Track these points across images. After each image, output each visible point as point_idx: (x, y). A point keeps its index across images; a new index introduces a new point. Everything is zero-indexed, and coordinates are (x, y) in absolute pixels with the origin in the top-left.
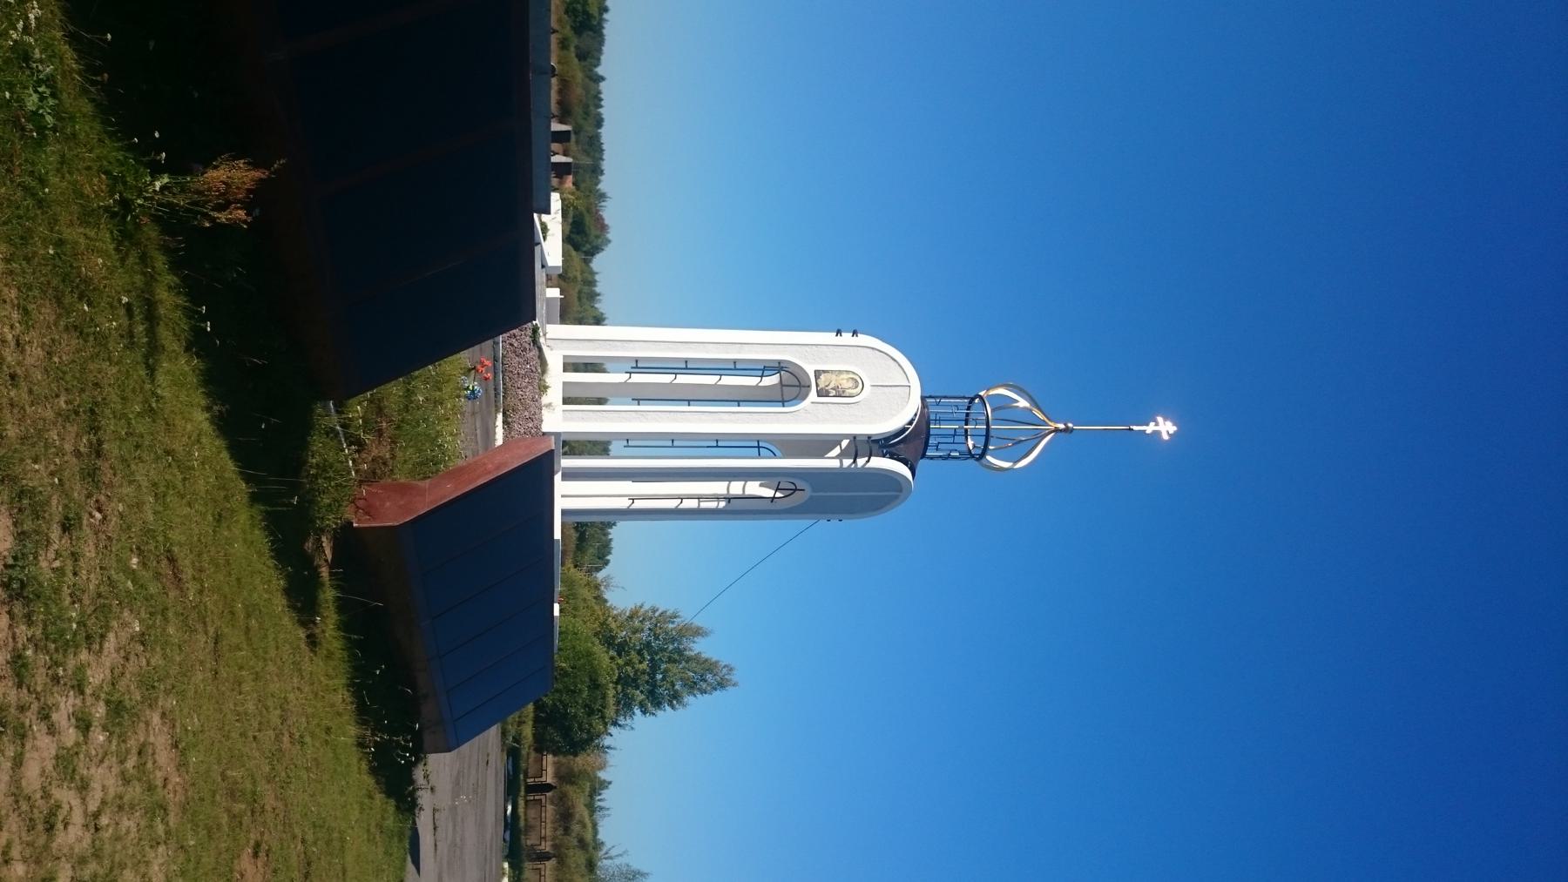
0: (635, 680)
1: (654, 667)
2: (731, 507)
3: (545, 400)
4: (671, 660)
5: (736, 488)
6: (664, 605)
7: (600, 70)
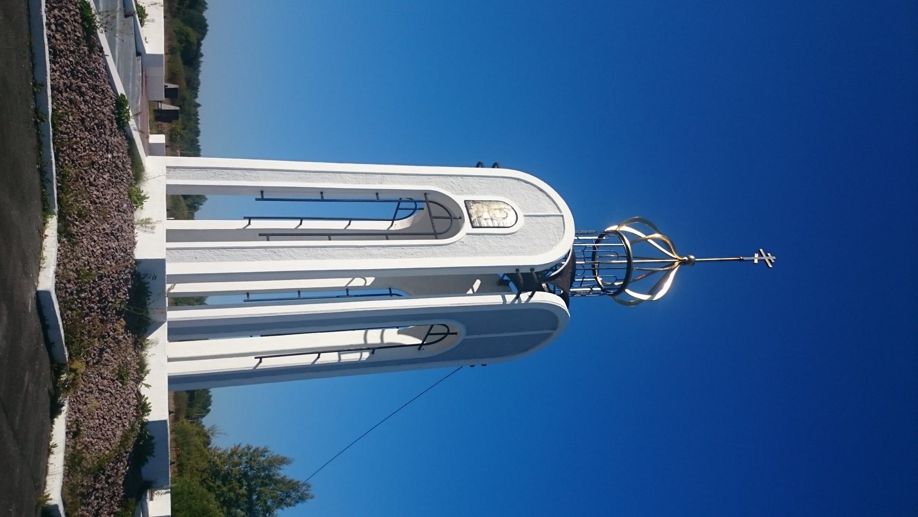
0: (237, 501)
1: (251, 491)
2: (376, 358)
3: (140, 215)
4: (264, 485)
5: (374, 336)
6: (257, 443)
7: (197, 101)
